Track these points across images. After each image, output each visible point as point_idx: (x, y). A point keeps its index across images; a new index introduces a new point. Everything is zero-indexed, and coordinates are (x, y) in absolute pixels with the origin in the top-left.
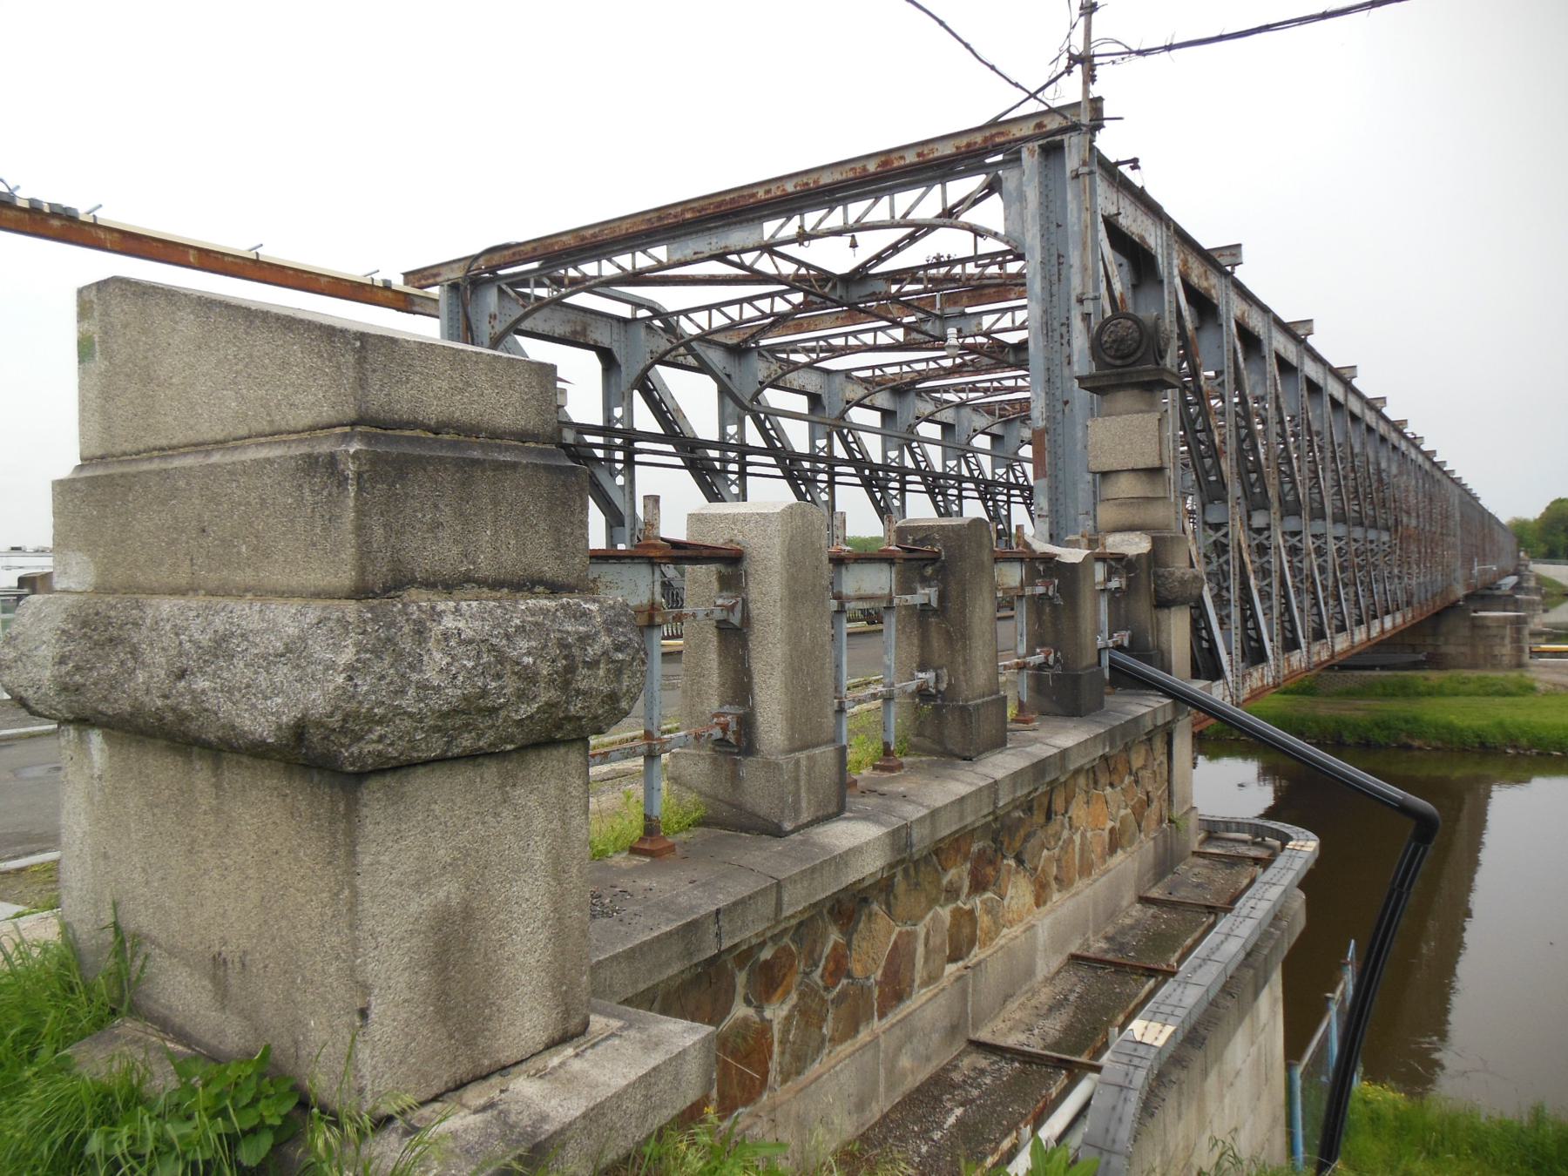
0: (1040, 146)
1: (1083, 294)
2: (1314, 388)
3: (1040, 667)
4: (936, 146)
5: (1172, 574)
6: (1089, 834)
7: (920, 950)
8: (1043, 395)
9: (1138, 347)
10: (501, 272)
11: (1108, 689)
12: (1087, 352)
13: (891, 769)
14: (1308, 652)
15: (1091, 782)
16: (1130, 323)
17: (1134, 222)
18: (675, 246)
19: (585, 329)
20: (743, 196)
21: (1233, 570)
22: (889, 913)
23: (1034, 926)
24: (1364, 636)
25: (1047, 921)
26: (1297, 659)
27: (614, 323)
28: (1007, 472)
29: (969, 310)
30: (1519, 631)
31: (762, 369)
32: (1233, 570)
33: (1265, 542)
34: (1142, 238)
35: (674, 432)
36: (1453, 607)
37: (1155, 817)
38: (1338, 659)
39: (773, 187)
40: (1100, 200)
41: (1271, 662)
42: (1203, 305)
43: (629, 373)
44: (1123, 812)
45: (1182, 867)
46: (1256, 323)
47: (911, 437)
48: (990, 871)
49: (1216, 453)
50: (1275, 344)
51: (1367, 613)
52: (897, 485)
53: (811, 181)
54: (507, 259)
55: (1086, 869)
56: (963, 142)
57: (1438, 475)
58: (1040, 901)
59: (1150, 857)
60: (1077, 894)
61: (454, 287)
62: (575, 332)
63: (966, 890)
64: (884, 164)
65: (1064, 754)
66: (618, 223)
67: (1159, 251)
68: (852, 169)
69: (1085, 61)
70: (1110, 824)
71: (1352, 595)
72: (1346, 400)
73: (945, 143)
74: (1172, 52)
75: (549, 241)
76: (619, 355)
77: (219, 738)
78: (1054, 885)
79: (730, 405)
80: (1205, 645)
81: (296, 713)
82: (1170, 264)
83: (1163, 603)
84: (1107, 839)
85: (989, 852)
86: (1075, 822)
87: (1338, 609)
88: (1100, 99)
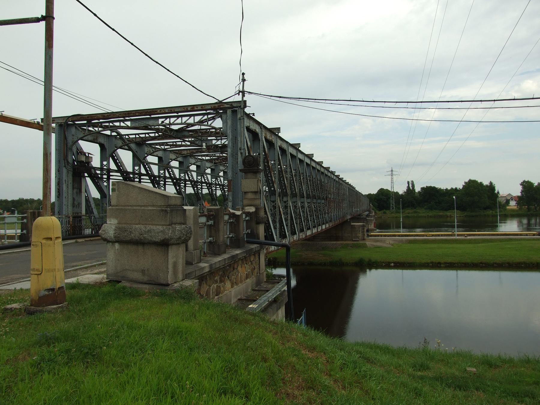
0: (231, 110)
1: (241, 148)
2: (301, 161)
3: (232, 237)
4: (206, 106)
5: (260, 216)
6: (242, 274)
7: (211, 292)
8: (231, 171)
10: (77, 122)
11: (246, 243)
12: (242, 162)
13: (206, 257)
14: (299, 235)
15: (242, 262)
16: (251, 157)
17: (254, 127)
19: (97, 138)
21: (277, 213)
22: (206, 284)
23: (231, 291)
24: (316, 231)
25: (234, 291)
26: (295, 237)
27: (105, 136)
28: (216, 180)
30: (363, 229)
31: (146, 149)
32: (277, 213)
33: (287, 205)
34: (255, 130)
35: (121, 169)
36: (346, 222)
37: (256, 272)
38: (307, 238)
39: (162, 110)
40: (245, 123)
41: (288, 238)
42: (271, 144)
43: (108, 153)
44: (249, 270)
45: (262, 285)
46: (284, 146)
47: (188, 170)
48: (223, 278)
49: (273, 183)
50: (290, 151)
51: (317, 224)
52: (183, 185)
53: (173, 110)
55: (241, 282)
56: (213, 106)
57: (341, 182)
58: (232, 287)
59: (255, 281)
60: (239, 286)
61: (60, 126)
62: (94, 139)
63: (219, 281)
65: (237, 254)
67: (259, 132)
70: (246, 273)
71: (312, 219)
72: (311, 164)
75: (93, 115)
76: (106, 147)
78: (235, 284)
79: (136, 160)
80: (270, 233)
81: (164, 238)
82: (262, 136)
83: (258, 223)
84: (245, 276)
85: (223, 275)
86: (239, 271)
87: (319, 221)
88: (246, 101)
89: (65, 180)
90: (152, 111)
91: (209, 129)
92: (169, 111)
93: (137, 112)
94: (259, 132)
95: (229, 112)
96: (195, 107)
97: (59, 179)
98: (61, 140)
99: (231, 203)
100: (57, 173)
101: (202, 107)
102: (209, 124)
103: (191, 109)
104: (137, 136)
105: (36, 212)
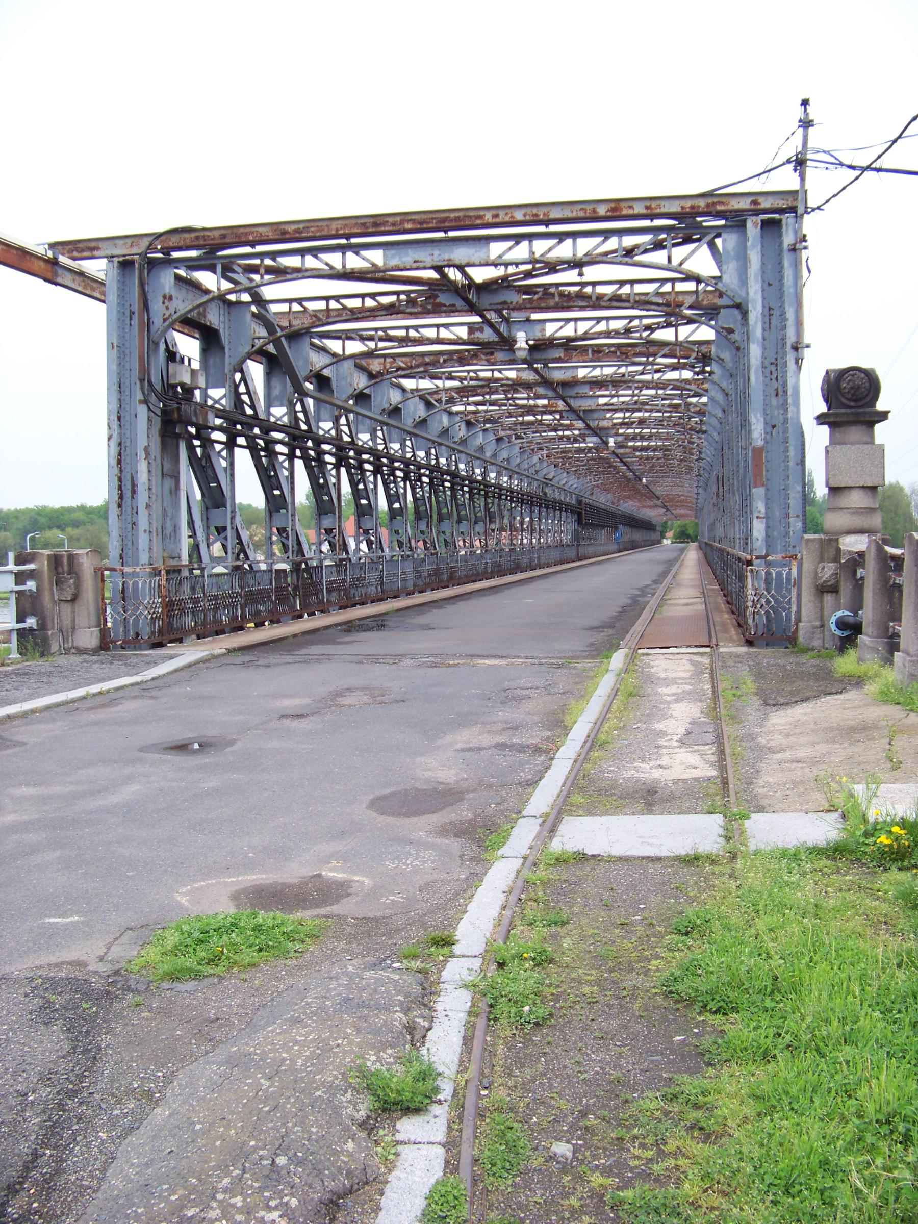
4: (663, 203)
9: (869, 393)
18: (393, 252)
20: (470, 217)
29: (535, 316)
39: (502, 213)
54: (188, 243)
56: (688, 204)
61: (126, 265)
64: (614, 210)
66: (325, 224)
68: (581, 209)
69: (800, 163)
73: (672, 202)
74: (880, 173)
75: (242, 230)
77: (690, 723)
89: (146, 449)
90: (465, 216)
91: (673, 281)
92: (528, 218)
93: (409, 217)
94: (222, 326)
95: (753, 227)
96: (622, 204)
97: (120, 444)
98: (124, 313)
99: (762, 522)
100: (115, 425)
101: (647, 208)
102: (675, 262)
103: (608, 211)
104: (333, 305)
105: (62, 556)
